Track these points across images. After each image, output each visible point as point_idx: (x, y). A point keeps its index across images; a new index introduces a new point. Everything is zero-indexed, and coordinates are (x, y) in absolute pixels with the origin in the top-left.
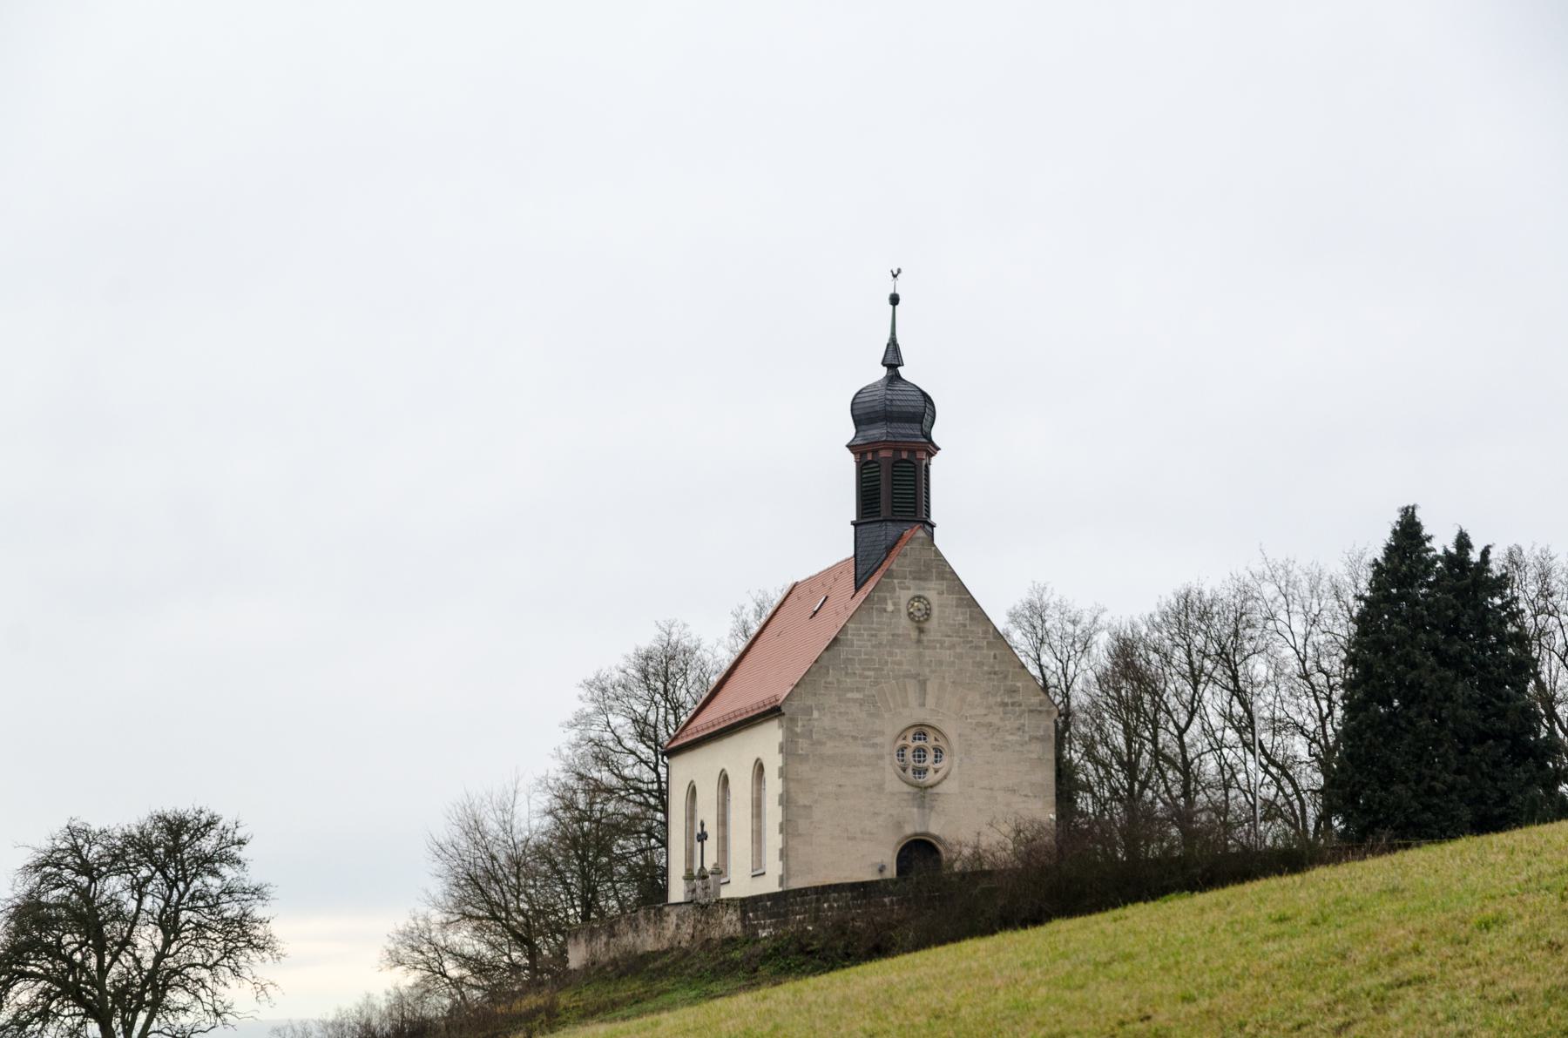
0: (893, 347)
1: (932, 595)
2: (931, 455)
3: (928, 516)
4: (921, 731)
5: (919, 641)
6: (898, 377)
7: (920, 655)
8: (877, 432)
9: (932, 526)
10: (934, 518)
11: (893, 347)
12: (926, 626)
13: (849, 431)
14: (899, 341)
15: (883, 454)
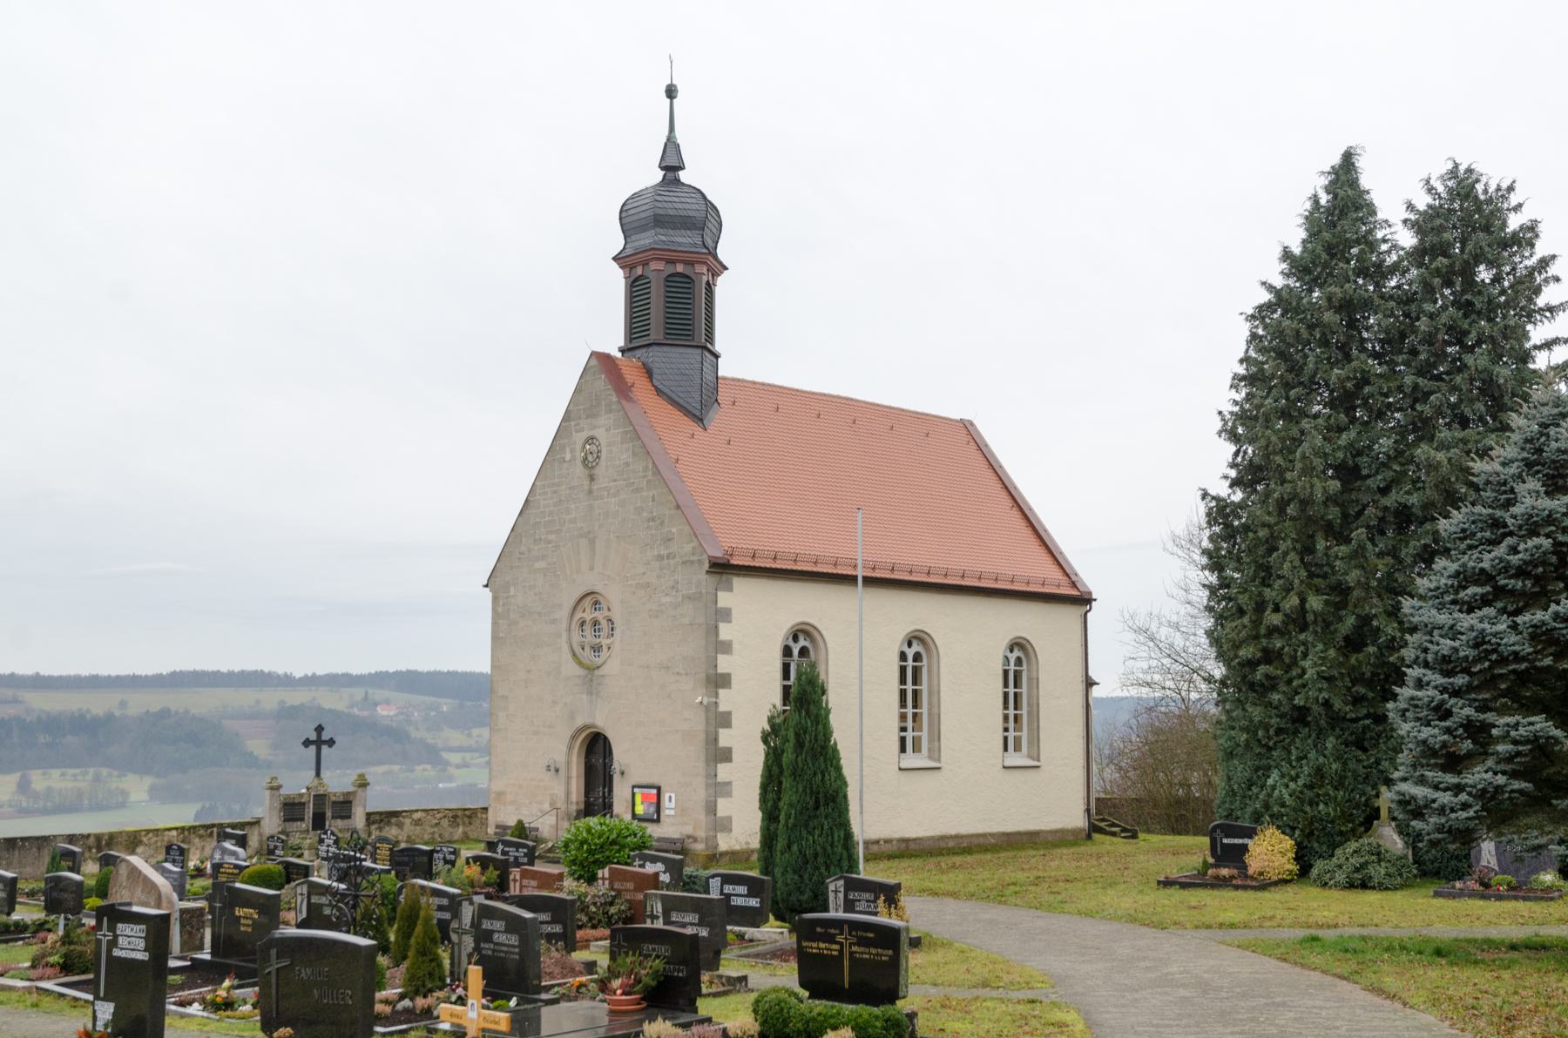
0: (671, 146)
1: (600, 433)
2: (715, 275)
3: (710, 336)
4: (591, 598)
5: (590, 492)
6: (677, 181)
7: (591, 507)
8: (646, 239)
9: (717, 356)
10: (719, 347)
11: (671, 146)
12: (596, 471)
13: (617, 242)
14: (680, 137)
15: (654, 265)
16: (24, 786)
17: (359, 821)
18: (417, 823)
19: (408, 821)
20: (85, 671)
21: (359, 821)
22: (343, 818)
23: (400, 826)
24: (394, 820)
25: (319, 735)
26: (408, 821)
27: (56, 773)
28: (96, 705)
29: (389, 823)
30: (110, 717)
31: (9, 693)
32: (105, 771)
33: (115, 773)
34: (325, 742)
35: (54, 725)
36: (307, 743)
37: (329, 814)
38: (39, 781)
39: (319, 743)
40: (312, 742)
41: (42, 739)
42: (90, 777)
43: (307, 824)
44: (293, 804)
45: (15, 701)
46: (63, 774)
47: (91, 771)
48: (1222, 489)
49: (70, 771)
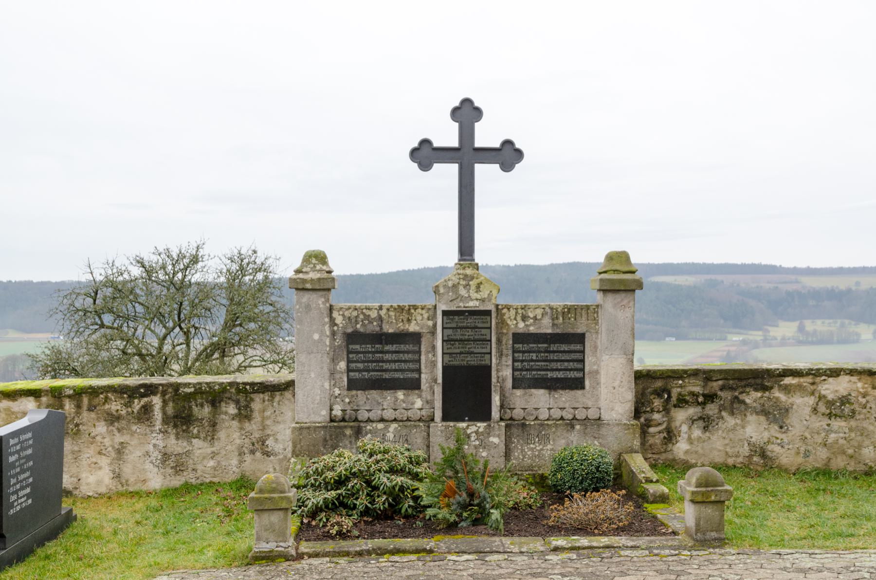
16: (801, 329)
17: (610, 394)
18: (839, 408)
19: (802, 403)
20: (835, 265)
21: (610, 394)
22: (552, 385)
23: (777, 415)
24: (752, 397)
25: (466, 134)
26: (802, 403)
27: (819, 322)
28: (841, 283)
29: (736, 406)
30: (849, 291)
31: (793, 277)
32: (847, 321)
33: (853, 323)
34: (488, 154)
35: (816, 295)
36: (425, 154)
37: (503, 371)
38: (809, 326)
39: (466, 156)
40: (445, 154)
41: (811, 303)
42: (838, 324)
43: (429, 397)
44: (381, 338)
45: (797, 282)
46: (823, 323)
47: (839, 321)
48: (777, 461)
49: (827, 321)
